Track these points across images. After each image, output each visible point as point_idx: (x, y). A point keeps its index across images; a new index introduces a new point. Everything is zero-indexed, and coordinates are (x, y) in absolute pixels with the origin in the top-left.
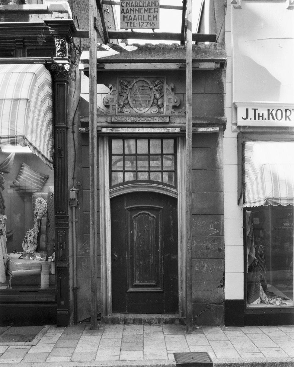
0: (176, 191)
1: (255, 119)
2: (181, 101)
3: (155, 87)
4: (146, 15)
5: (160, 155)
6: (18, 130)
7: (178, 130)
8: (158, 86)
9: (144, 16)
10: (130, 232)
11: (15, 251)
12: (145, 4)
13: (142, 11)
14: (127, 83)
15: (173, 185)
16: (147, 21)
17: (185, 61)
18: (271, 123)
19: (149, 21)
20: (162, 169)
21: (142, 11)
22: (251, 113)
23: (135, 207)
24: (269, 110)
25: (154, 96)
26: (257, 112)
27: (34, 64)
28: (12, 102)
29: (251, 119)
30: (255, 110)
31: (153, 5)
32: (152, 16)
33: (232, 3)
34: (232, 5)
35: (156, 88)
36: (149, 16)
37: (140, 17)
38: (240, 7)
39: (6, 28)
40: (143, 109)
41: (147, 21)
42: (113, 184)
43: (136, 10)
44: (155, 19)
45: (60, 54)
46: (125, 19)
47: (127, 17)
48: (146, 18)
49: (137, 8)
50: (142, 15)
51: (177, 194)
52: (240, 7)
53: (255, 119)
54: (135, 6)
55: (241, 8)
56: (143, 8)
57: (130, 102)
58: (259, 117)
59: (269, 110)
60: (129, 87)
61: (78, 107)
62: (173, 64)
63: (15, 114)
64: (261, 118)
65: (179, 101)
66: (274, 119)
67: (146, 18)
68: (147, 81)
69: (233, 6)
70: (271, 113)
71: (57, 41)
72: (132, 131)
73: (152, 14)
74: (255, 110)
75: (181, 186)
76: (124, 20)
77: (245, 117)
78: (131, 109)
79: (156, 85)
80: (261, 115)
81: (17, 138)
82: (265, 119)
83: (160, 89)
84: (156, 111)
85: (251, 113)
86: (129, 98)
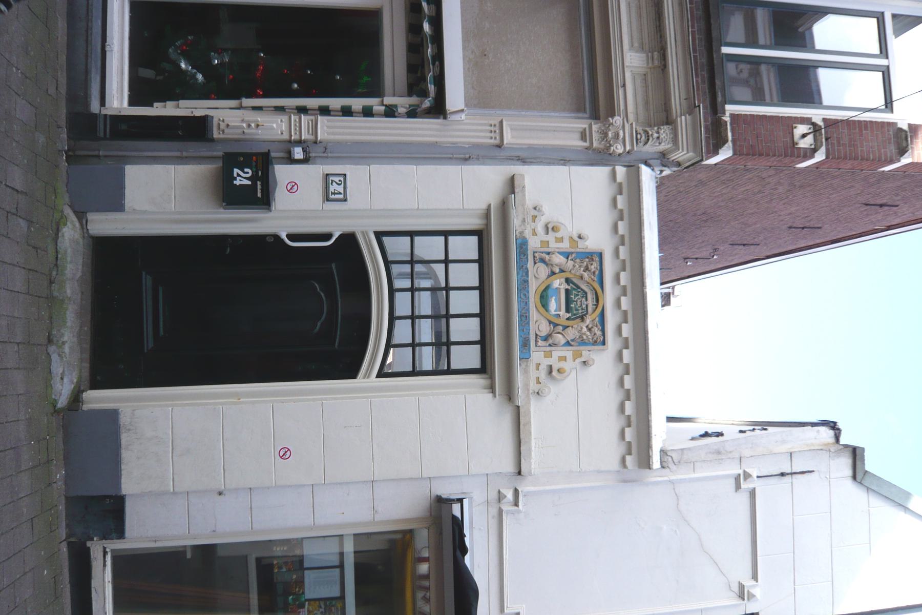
3: (587, 327)
5: (413, 342)
8: (588, 333)
11: (51, 282)
14: (593, 270)
23: (337, 304)
25: (568, 327)
27: (124, 203)
33: (745, 472)
34: (741, 472)
35: (585, 329)
38: (738, 487)
39: (696, 86)
42: (9, 214)
52: (738, 487)
55: (736, 491)
61: (609, 163)
69: (739, 475)
71: (890, 135)
79: (590, 330)
83: (583, 337)
84: (539, 331)
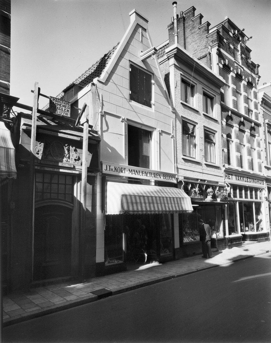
0: (73, 205)
1: (110, 171)
2: (79, 156)
4: (64, 108)
6: (12, 168)
7: (77, 172)
9: (62, 108)
10: (226, 204)
12: (63, 103)
13: (62, 106)
15: (71, 201)
16: (64, 112)
17: (82, 137)
18: (115, 173)
19: (65, 112)
20: (58, 191)
21: (62, 106)
22: (108, 167)
24: (115, 167)
26: (111, 167)
28: (5, 149)
29: (108, 170)
30: (110, 166)
31: (67, 104)
32: (67, 110)
36: (65, 109)
37: (60, 109)
40: (59, 158)
41: (64, 112)
43: (58, 104)
44: (68, 112)
45: (6, 115)
46: (52, 107)
47: (53, 106)
48: (63, 110)
49: (59, 103)
50: (62, 108)
51: (73, 207)
53: (110, 171)
54: (58, 102)
56: (62, 104)
57: (52, 153)
58: (111, 170)
59: (115, 167)
60: (51, 145)
62: (76, 137)
63: (9, 158)
64: (112, 171)
65: (78, 157)
66: (117, 172)
67: (63, 110)
68: (61, 143)
70: (116, 169)
72: (52, 170)
73: (67, 109)
74: (110, 166)
75: (178, 204)
76: (52, 108)
77: (106, 169)
78: (52, 157)
80: (112, 169)
81: (12, 173)
82: (114, 171)
85: (108, 167)
86: (51, 151)
